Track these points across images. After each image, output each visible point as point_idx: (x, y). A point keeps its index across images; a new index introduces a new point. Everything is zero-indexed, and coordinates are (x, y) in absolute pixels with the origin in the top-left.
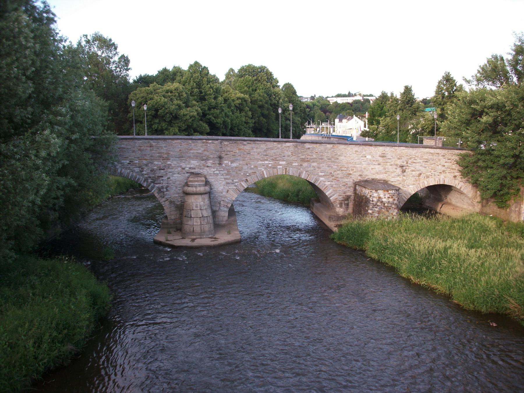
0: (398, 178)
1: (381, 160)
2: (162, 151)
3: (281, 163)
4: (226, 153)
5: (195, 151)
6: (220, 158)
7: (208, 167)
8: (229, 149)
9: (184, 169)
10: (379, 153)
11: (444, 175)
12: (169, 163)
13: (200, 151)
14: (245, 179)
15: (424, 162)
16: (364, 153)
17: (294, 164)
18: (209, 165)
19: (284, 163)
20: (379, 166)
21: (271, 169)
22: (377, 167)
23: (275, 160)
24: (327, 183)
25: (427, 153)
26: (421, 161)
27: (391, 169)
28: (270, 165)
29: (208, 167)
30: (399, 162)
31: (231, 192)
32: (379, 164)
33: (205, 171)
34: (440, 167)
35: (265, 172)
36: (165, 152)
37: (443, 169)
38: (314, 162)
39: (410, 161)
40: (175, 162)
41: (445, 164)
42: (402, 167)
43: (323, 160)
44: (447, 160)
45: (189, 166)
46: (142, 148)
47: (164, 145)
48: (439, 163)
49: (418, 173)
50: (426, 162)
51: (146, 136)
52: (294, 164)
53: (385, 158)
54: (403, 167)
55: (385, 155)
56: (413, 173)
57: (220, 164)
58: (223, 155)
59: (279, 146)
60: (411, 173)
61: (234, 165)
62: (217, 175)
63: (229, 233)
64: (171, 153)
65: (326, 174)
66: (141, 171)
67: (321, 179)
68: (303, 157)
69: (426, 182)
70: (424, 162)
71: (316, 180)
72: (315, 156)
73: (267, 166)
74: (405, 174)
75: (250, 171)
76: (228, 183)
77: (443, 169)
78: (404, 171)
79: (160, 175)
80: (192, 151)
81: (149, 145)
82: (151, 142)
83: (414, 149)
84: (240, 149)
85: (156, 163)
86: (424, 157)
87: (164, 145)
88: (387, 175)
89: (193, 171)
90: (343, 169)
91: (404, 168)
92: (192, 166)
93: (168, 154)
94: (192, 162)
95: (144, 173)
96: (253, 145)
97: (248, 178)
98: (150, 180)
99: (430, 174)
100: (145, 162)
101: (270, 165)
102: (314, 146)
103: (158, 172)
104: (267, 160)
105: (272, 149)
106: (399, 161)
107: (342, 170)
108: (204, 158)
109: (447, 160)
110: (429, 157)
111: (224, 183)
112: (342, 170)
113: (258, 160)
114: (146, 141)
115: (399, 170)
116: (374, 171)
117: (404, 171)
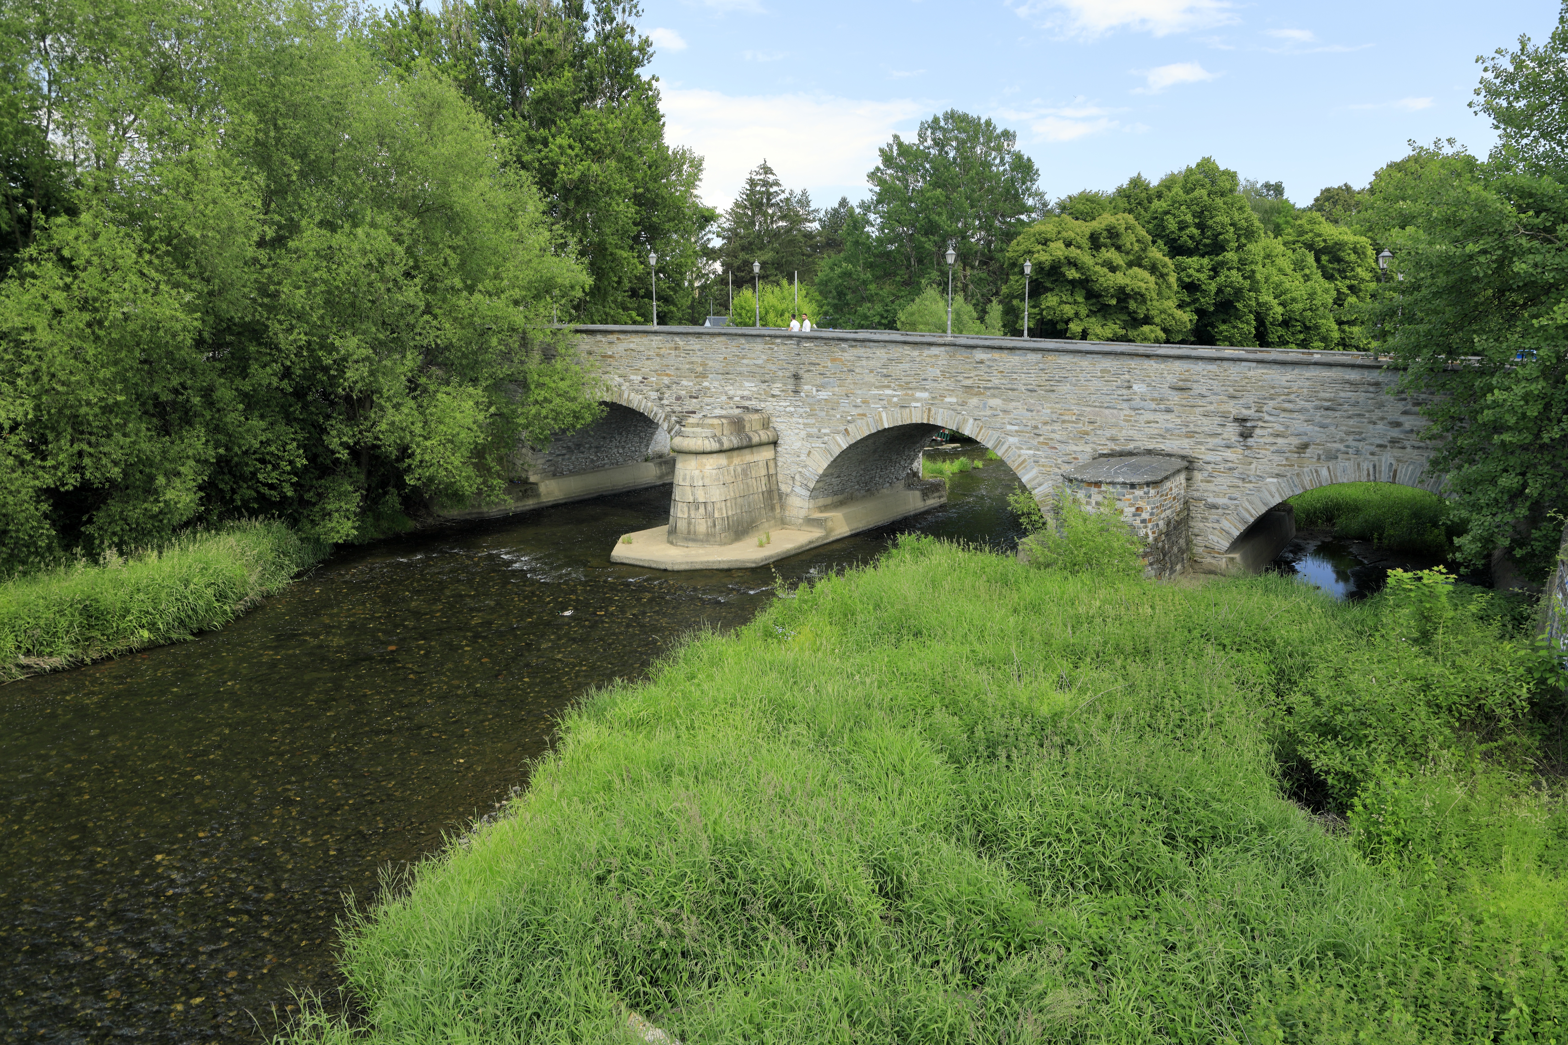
0: (1229, 454)
1: (1175, 398)
2: (694, 359)
3: (918, 394)
4: (807, 367)
5: (751, 362)
6: (796, 377)
7: (773, 396)
8: (813, 359)
9: (731, 398)
10: (1171, 379)
11: (1397, 453)
12: (706, 384)
13: (760, 362)
14: (842, 428)
15: (1317, 408)
16: (1127, 377)
17: (948, 400)
18: (776, 392)
19: (925, 395)
20: (1168, 416)
21: (898, 410)
22: (1161, 417)
23: (907, 386)
24: (1026, 453)
25: (1335, 381)
26: (1309, 405)
27: (1209, 425)
28: (895, 399)
29: (773, 396)
30: (1234, 409)
31: (816, 455)
32: (1169, 411)
33: (769, 406)
34: (1380, 426)
35: (884, 415)
36: (699, 360)
37: (1395, 433)
38: (994, 396)
39: (1271, 403)
40: (716, 384)
41: (1402, 419)
42: (1241, 421)
43: (1016, 393)
44: (1409, 407)
45: (739, 393)
46: (662, 351)
47: (698, 347)
48: (1378, 413)
49: (1295, 441)
50: (1327, 409)
51: (656, 327)
52: (948, 400)
53: (1185, 394)
54: (1245, 420)
55: (1188, 384)
56: (1280, 441)
57: (796, 392)
58: (801, 372)
59: (916, 353)
60: (1271, 440)
61: (823, 395)
62: (791, 414)
63: (92, 615)
64: (711, 363)
65: (1022, 428)
66: (661, 399)
67: (1012, 440)
68: (968, 382)
69: (1324, 472)
70: (1317, 408)
71: (999, 443)
72: (996, 381)
73: (889, 402)
74: (1250, 441)
75: (855, 412)
76: (809, 436)
77: (1395, 433)
78: (1246, 435)
79: (691, 409)
80: (745, 361)
81: (672, 345)
82: (677, 339)
83: (1289, 368)
84: (833, 360)
85: (685, 382)
86: (1322, 395)
87: (698, 347)
88: (1191, 441)
89: (747, 403)
90: (1066, 418)
91: (1249, 424)
92: (746, 393)
93: (704, 365)
94: (747, 384)
95: (665, 402)
96: (860, 351)
97: (851, 428)
98: (674, 419)
99: (1341, 447)
100: (666, 380)
101: (895, 399)
102: (996, 355)
103: (687, 401)
104: (889, 387)
105: (899, 361)
106: (1232, 402)
107: (1064, 422)
108: (767, 377)
109: (1409, 407)
110: (1342, 394)
111: (803, 434)
112: (1064, 422)
113: (870, 386)
114: (669, 337)
115: (1231, 432)
116: (1153, 430)
117: (1246, 435)
